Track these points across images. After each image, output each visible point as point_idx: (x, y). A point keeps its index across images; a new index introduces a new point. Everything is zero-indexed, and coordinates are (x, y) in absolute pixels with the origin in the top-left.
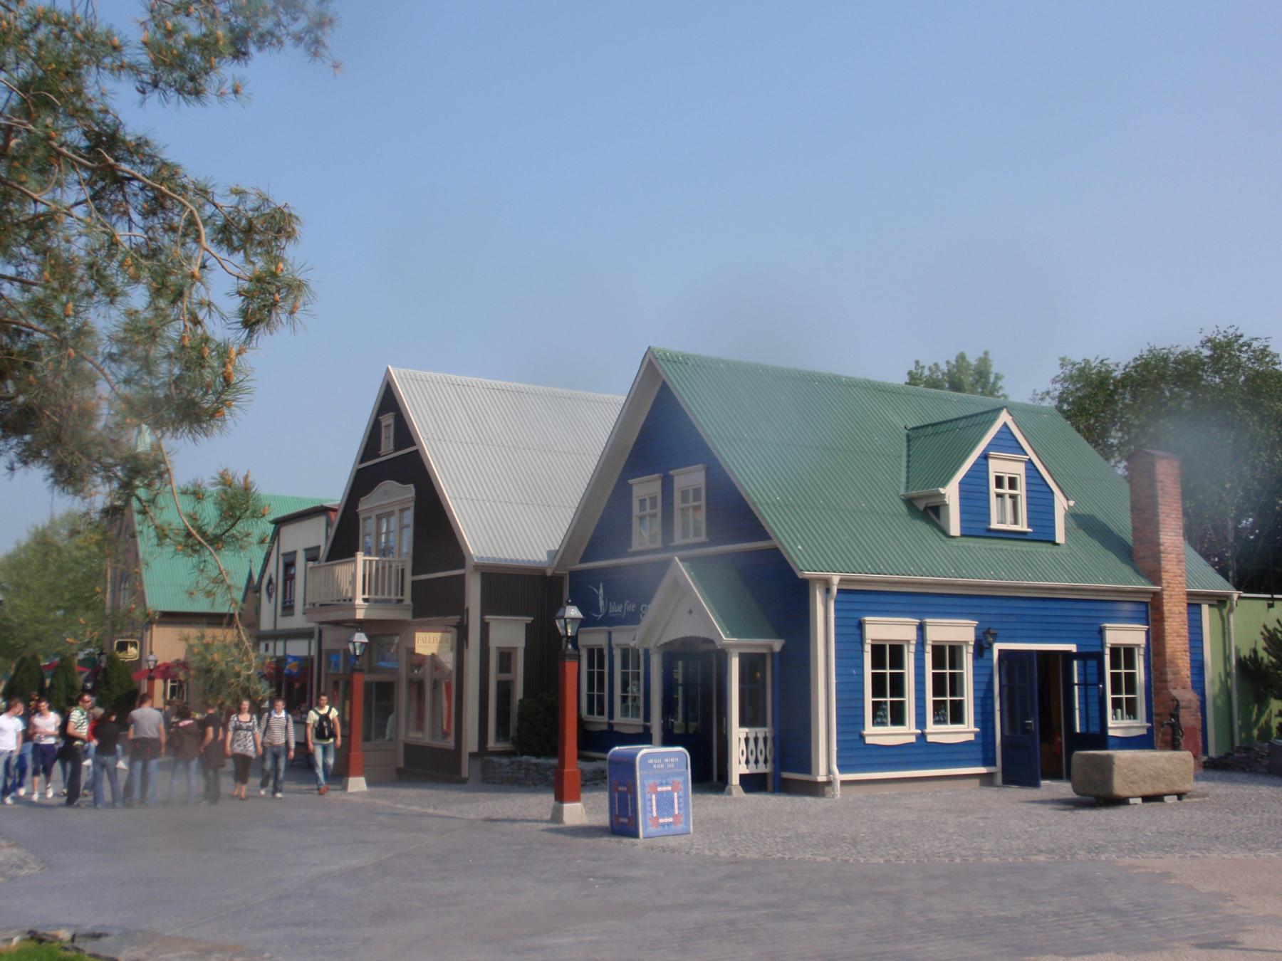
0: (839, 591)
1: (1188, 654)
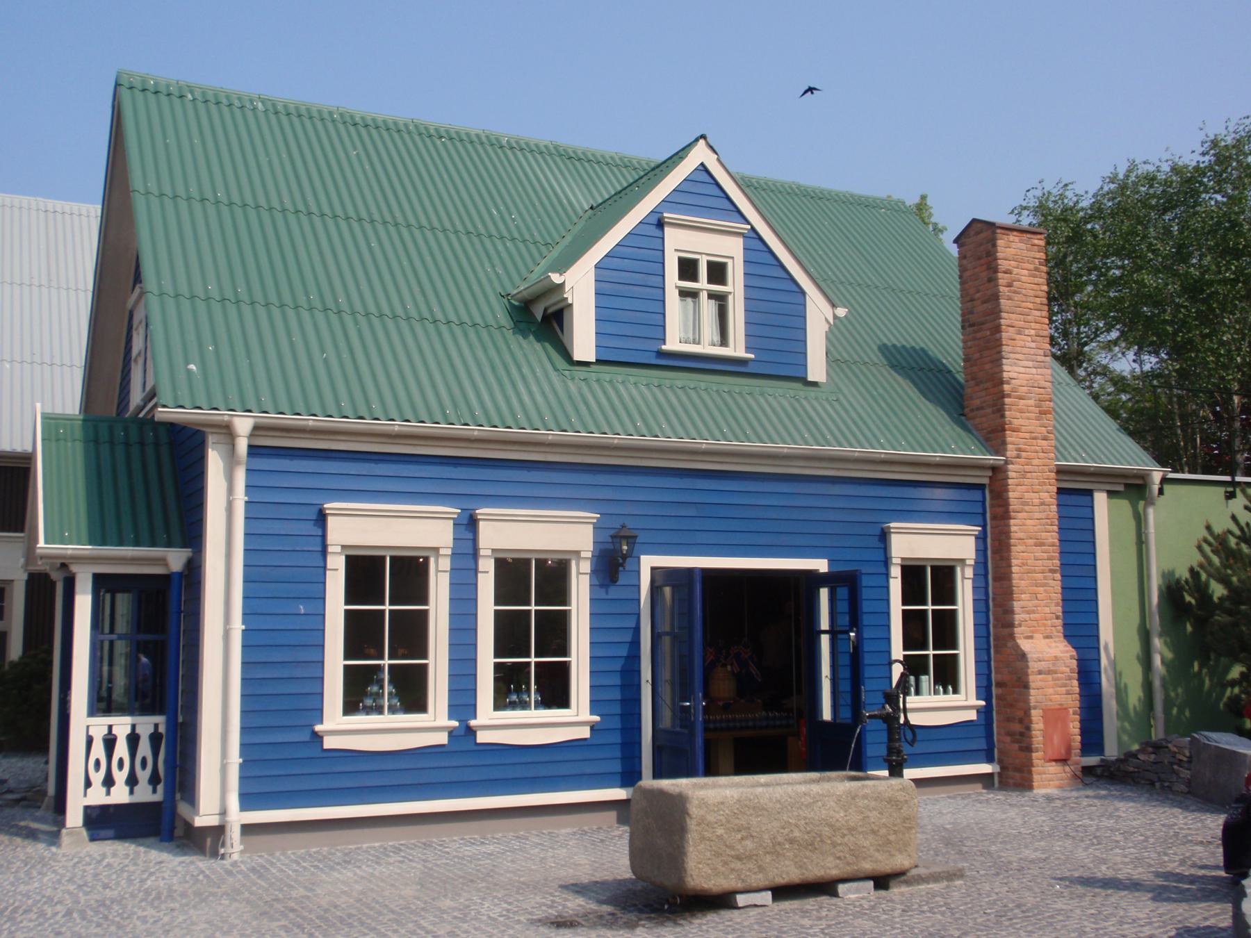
0: (254, 450)
1: (1058, 576)
